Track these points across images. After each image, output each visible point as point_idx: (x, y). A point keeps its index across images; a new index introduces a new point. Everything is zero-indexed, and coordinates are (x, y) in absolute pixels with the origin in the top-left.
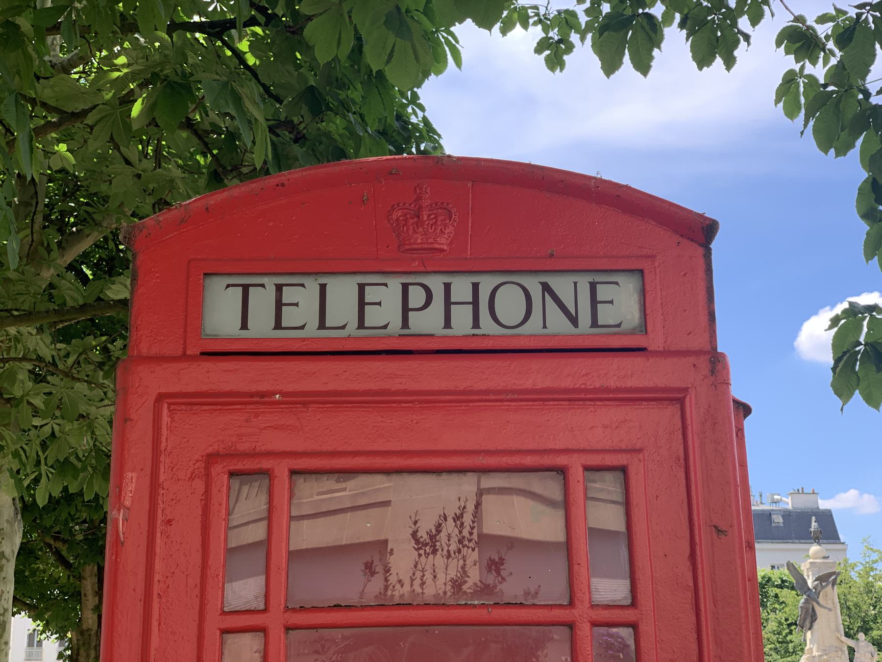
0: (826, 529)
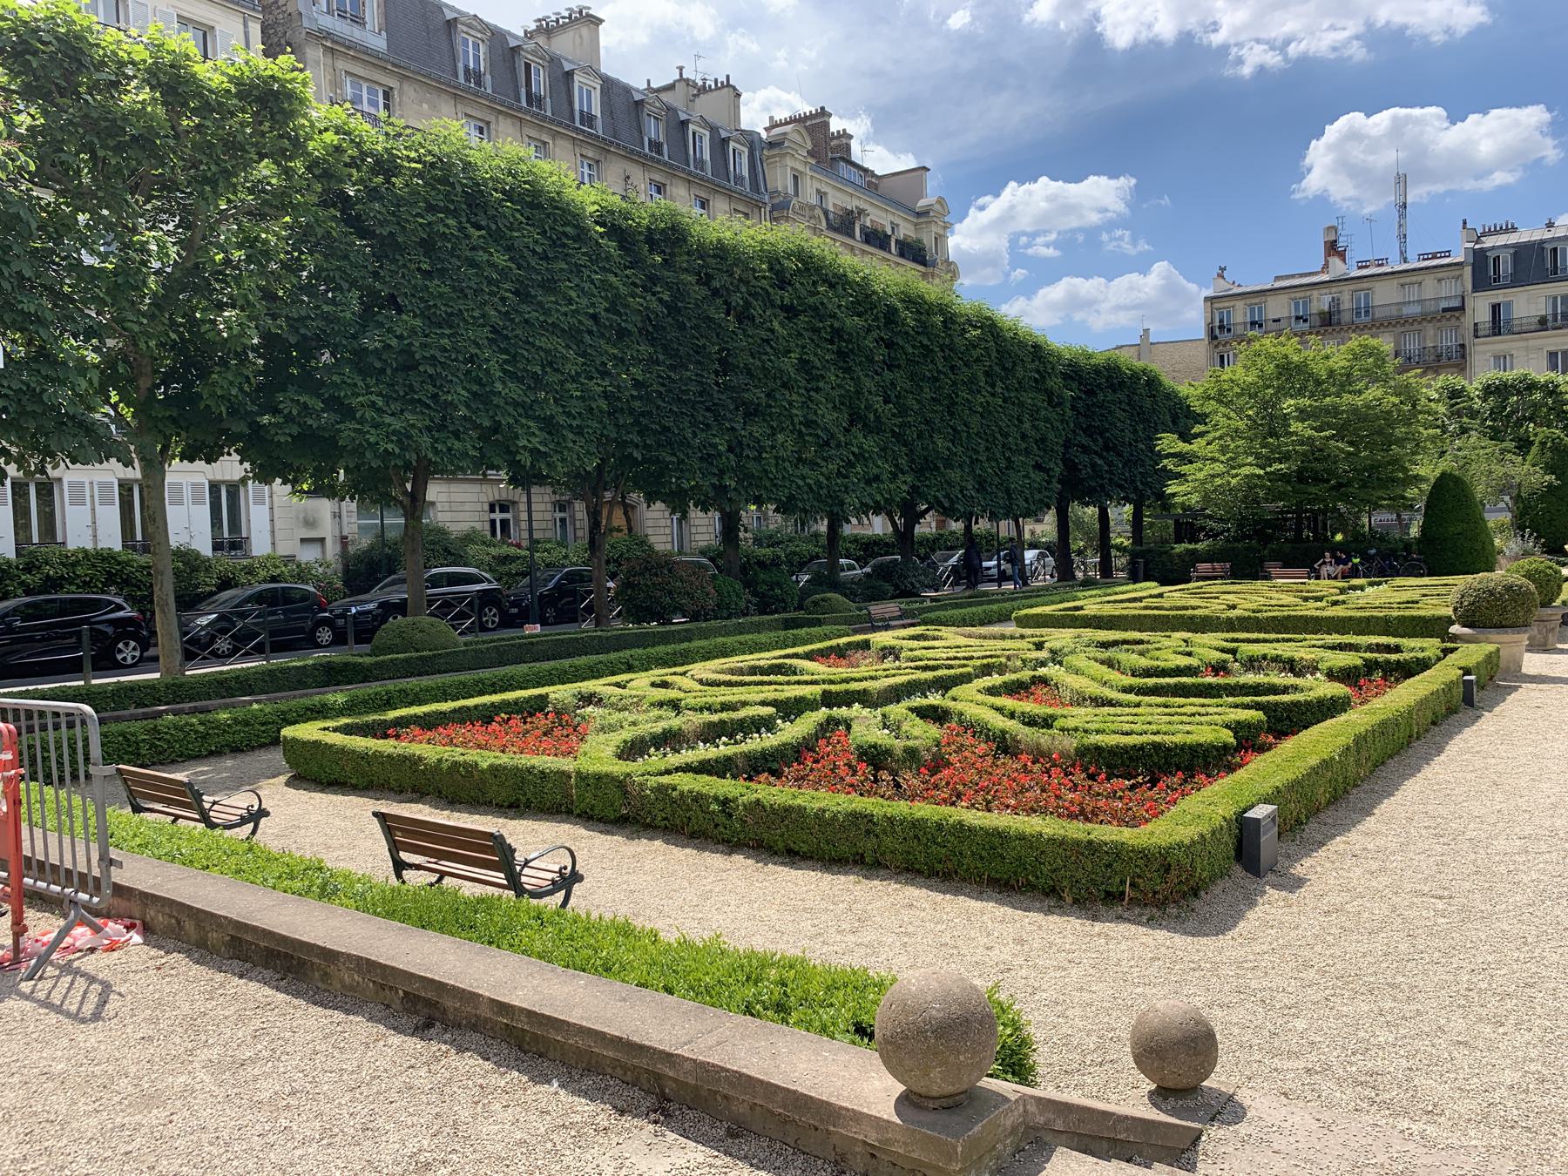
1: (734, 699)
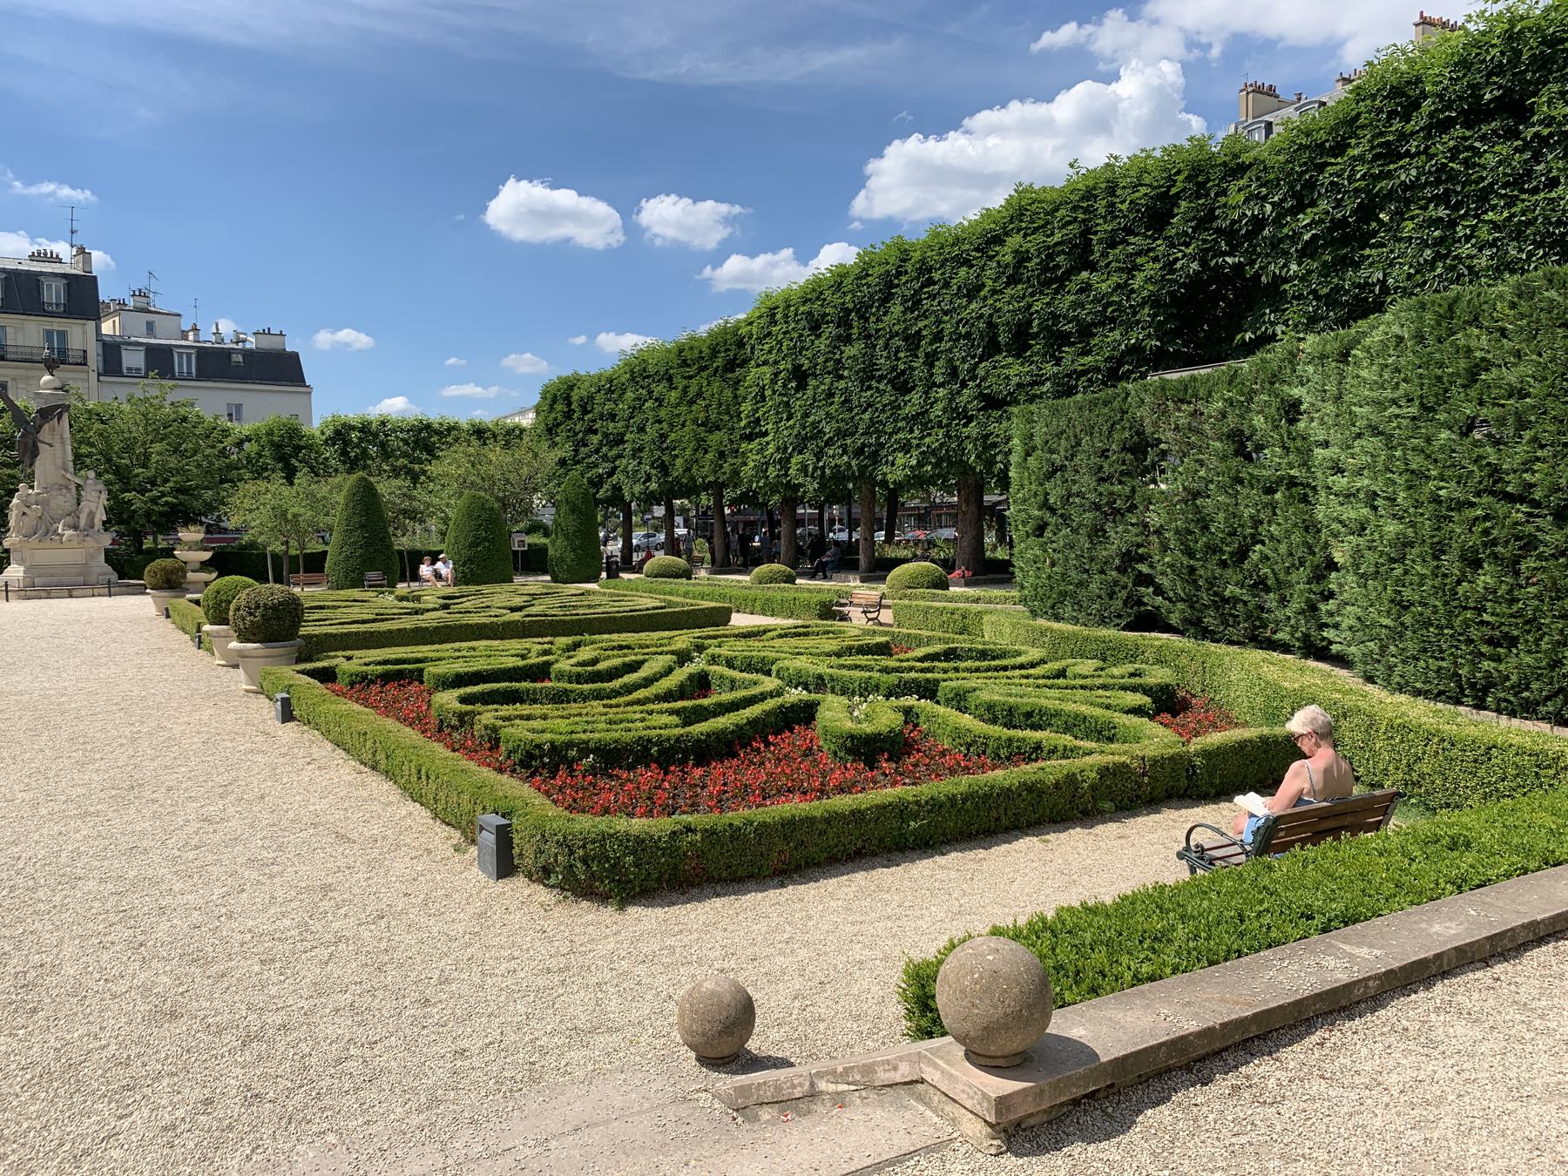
0: (278, 368)
1: (420, 655)
